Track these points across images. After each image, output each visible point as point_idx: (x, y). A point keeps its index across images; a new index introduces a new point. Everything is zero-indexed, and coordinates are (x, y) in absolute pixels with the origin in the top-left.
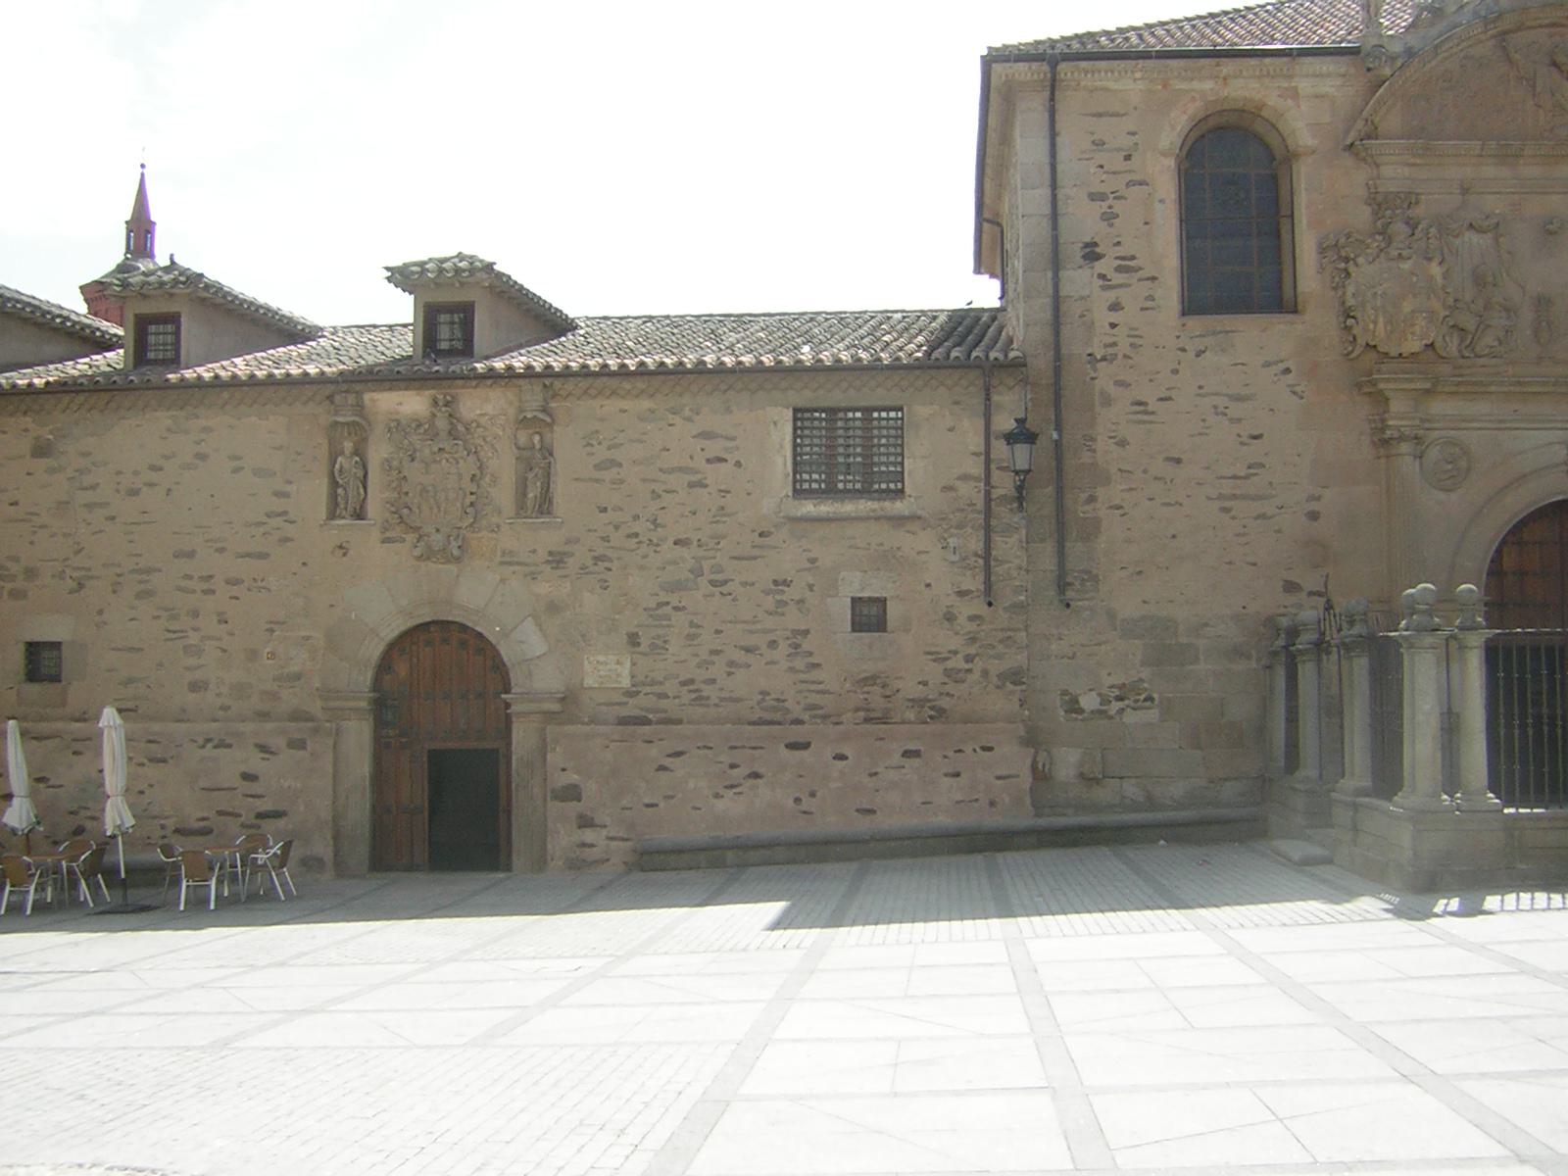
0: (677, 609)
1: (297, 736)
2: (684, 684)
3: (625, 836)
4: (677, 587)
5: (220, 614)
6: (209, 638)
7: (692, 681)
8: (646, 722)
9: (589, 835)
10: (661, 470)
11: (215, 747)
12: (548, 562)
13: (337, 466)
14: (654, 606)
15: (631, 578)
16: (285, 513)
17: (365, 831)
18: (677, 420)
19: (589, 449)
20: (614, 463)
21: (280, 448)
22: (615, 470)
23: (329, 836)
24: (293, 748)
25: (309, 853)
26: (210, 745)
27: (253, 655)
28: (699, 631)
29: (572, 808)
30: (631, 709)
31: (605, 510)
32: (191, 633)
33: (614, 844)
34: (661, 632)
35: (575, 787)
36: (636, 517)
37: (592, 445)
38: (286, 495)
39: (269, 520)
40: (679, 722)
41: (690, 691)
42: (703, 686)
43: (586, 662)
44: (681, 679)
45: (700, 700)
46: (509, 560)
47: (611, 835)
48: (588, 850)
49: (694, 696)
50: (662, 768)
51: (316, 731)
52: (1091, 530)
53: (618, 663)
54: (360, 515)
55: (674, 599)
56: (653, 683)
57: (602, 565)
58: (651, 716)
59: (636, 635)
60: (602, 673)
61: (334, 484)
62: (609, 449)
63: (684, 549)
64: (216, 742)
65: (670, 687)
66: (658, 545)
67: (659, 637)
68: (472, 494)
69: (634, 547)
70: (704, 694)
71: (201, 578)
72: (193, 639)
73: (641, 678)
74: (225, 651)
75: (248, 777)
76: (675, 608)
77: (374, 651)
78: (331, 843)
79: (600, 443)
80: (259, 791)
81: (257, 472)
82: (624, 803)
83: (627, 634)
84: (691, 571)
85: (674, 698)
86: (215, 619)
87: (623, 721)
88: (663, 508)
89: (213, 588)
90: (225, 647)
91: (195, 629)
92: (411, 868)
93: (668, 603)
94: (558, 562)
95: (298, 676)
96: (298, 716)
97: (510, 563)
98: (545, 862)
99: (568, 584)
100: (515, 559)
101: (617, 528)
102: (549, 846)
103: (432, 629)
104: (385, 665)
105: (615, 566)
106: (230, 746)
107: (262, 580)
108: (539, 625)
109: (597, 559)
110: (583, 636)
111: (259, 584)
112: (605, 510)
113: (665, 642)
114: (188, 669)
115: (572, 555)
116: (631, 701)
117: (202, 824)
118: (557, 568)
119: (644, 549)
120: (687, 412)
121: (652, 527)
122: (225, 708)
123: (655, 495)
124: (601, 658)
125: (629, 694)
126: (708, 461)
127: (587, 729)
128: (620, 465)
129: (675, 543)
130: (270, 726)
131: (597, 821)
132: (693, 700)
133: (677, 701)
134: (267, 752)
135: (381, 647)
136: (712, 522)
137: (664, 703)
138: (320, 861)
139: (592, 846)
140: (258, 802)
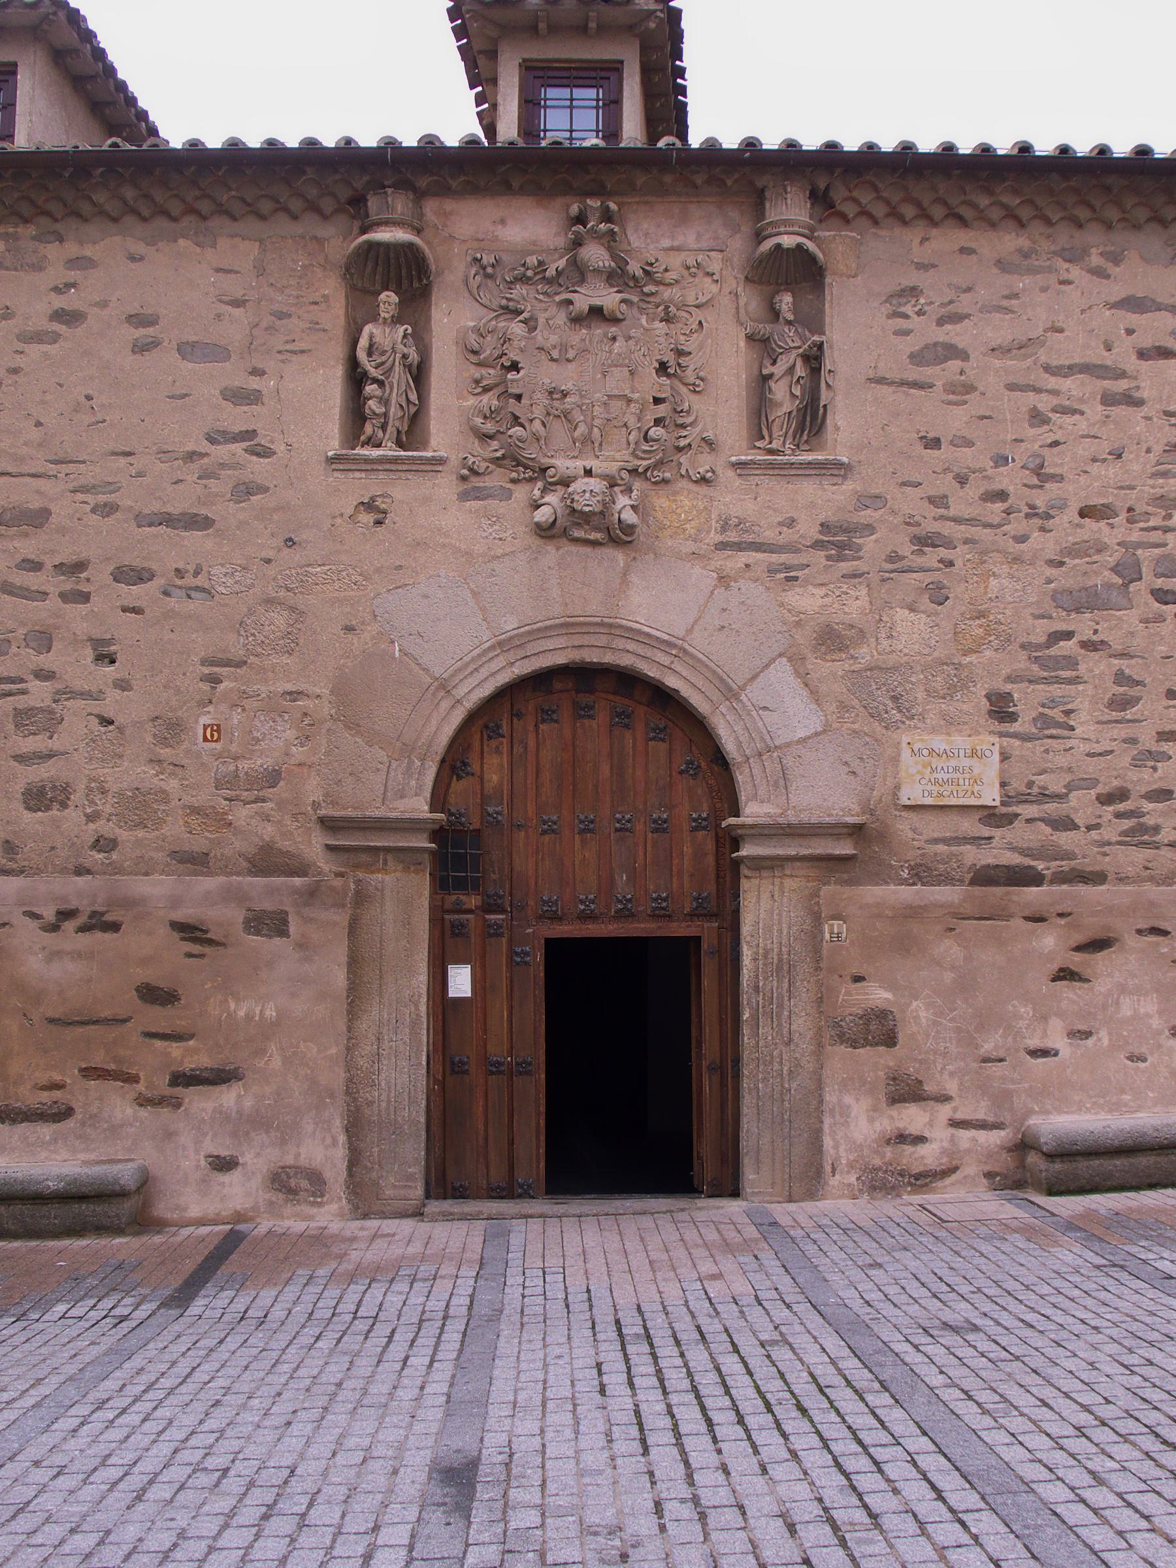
0: (1089, 646)
1: (268, 905)
2: (1106, 799)
3: (991, 1119)
4: (1086, 601)
5: (97, 643)
6: (73, 694)
7: (1121, 795)
8: (1033, 878)
9: (913, 1118)
10: (1047, 369)
11: (83, 929)
12: (817, 545)
13: (363, 342)
14: (1043, 639)
15: (993, 582)
16: (250, 434)
17: (414, 1113)
18: (1075, 272)
19: (900, 323)
20: (952, 352)
21: (238, 303)
22: (954, 365)
23: (338, 1124)
24: (258, 933)
25: (289, 1160)
26: (69, 926)
27: (171, 729)
28: (1134, 692)
29: (876, 1061)
30: (1000, 852)
31: (935, 443)
32: (34, 685)
33: (965, 1135)
34: (1056, 690)
35: (882, 1015)
36: (1001, 460)
37: (906, 317)
38: (253, 398)
39: (211, 449)
40: (1098, 878)
41: (1119, 815)
42: (1148, 806)
43: (906, 753)
44: (1101, 789)
45: (1141, 834)
46: (738, 540)
47: (960, 1116)
48: (908, 1149)
49: (1127, 824)
50: (1065, 975)
51: (311, 895)
52: (546, 715)
53: (974, 753)
54: (412, 433)
55: (1084, 625)
56: (1045, 796)
57: (931, 557)
58: (1040, 866)
59: (1007, 697)
60: (941, 776)
61: (356, 378)
62: (941, 322)
63: (1102, 524)
64: (81, 920)
65: (1081, 806)
66: (1048, 517)
67: (1052, 703)
68: (657, 401)
69: (996, 520)
70: (1149, 821)
71: (59, 568)
72: (39, 693)
73: (1017, 785)
74: (107, 722)
75: (153, 995)
76: (1084, 645)
77: (444, 726)
78: (342, 1138)
79: (920, 313)
80: (181, 1024)
81: (187, 350)
82: (988, 1047)
83: (988, 697)
84: (1115, 570)
85: (1089, 828)
86: (89, 654)
87: (985, 877)
88: (1056, 444)
89: (85, 588)
90: (109, 714)
91: (43, 675)
92: (508, 1191)
93: (1069, 635)
94: (841, 546)
95: (273, 777)
96: (268, 861)
97: (739, 547)
98: (819, 1173)
99: (864, 591)
100: (750, 538)
101: (962, 480)
102: (828, 1142)
103: (558, 685)
104: (455, 763)
105: (960, 554)
106: (115, 927)
107: (196, 574)
108: (803, 677)
109: (924, 542)
110: (895, 699)
111: (189, 581)
112: (935, 443)
113: (1068, 713)
114: (20, 758)
115: (870, 529)
116: (997, 833)
117: (45, 1097)
118: (840, 558)
119: (1017, 525)
120: (1095, 260)
121: (1035, 481)
122: (104, 844)
123: (1037, 418)
124: (939, 743)
125: (991, 816)
126: (1142, 355)
127: (906, 894)
128: (964, 355)
129: (1083, 514)
130: (209, 884)
131: (929, 1088)
132: (1125, 833)
133: (1094, 834)
134: (196, 940)
135: (458, 717)
136: (1154, 475)
137: (1065, 839)
138: (316, 1180)
139: (920, 1139)
140: (175, 1049)
